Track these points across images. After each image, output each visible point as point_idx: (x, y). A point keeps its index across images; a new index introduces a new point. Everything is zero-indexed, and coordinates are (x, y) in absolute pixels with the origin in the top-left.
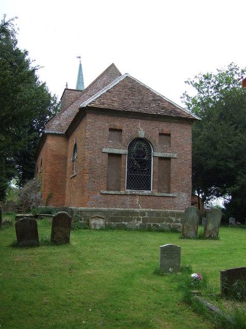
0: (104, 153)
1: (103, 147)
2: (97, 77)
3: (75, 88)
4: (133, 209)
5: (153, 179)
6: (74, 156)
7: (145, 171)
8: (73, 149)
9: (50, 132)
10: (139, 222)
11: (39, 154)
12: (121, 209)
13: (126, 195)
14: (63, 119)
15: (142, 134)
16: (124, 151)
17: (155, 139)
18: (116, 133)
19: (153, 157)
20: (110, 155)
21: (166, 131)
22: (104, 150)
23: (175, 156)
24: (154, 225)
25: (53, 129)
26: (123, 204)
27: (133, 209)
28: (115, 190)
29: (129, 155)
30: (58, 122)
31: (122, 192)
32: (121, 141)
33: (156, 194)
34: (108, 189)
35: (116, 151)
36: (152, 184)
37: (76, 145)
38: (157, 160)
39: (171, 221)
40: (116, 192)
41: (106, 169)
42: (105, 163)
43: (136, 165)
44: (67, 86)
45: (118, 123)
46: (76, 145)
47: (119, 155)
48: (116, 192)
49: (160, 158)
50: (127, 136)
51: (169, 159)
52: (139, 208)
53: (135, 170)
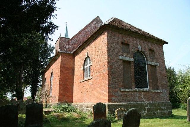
0: (120, 59)
1: (119, 55)
2: (89, 23)
3: (65, 37)
4: (141, 102)
5: (149, 80)
6: (84, 66)
7: (143, 74)
8: (83, 62)
9: (63, 52)
10: (145, 112)
11: (48, 70)
12: (134, 103)
13: (136, 92)
14: (71, 44)
15: (140, 48)
16: (132, 59)
17: (147, 53)
18: (125, 47)
19: (147, 64)
20: (124, 61)
21: (152, 48)
22: (120, 57)
23: (158, 64)
24: (153, 113)
25: (65, 50)
26: (134, 99)
27: (141, 102)
28: (129, 88)
29: (134, 63)
30: (67, 46)
31: (133, 90)
32: (129, 52)
33: (153, 91)
34: (125, 88)
35: (127, 59)
36: (148, 84)
37: (52, 72)
38: (150, 67)
39: (161, 109)
40: (130, 90)
41: (122, 72)
42: (121, 67)
43: (138, 70)
44: (60, 35)
45: (126, 40)
46: (52, 72)
47: (129, 62)
48: (130, 90)
49: (152, 66)
50: (132, 49)
51: (155, 66)
52: (144, 101)
53: (138, 74)
